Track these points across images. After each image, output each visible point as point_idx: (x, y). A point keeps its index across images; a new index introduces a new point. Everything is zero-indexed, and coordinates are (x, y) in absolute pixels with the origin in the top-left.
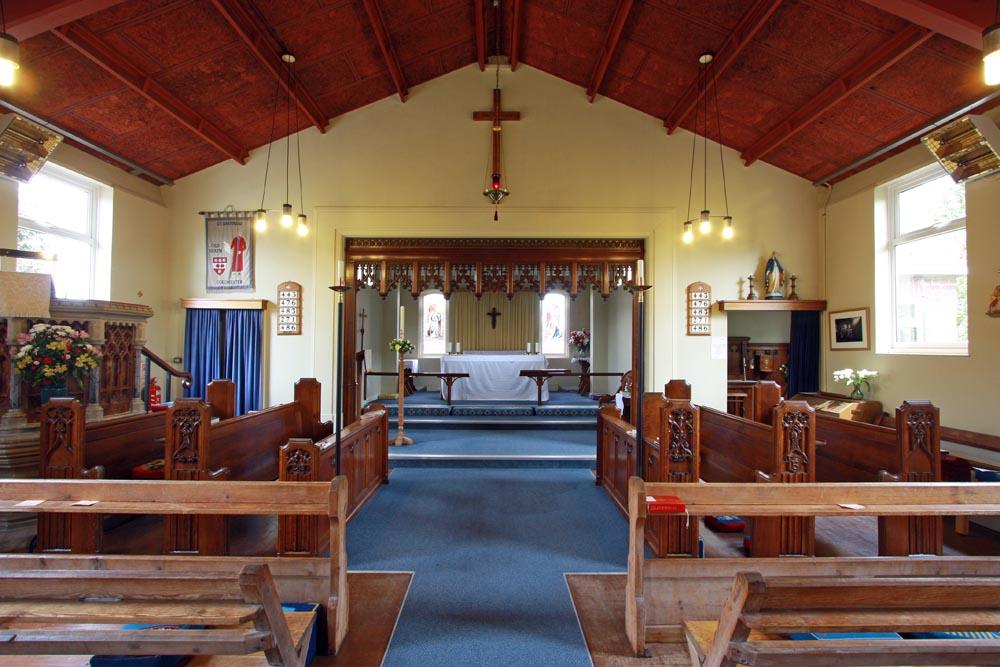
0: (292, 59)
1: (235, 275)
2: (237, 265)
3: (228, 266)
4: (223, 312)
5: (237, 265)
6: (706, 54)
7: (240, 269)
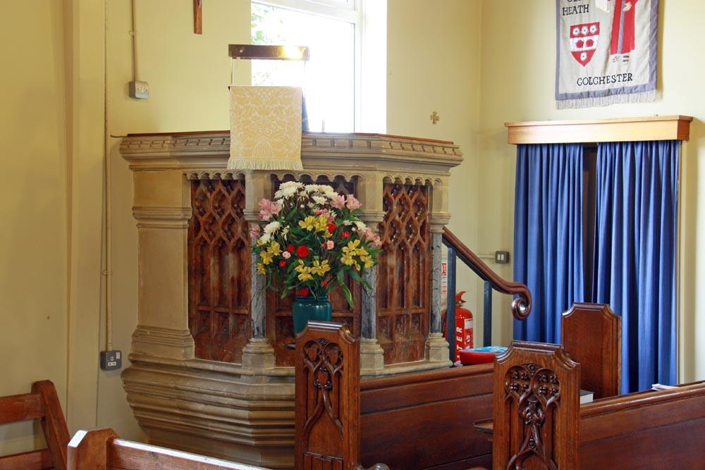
1: (617, 65)
2: (622, 39)
3: (601, 42)
4: (589, 149)
5: (622, 39)
7: (628, 46)
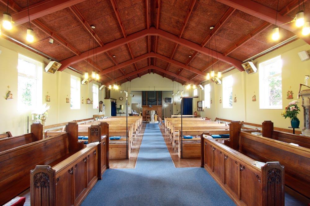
0: (94, 27)
6: (211, 27)
